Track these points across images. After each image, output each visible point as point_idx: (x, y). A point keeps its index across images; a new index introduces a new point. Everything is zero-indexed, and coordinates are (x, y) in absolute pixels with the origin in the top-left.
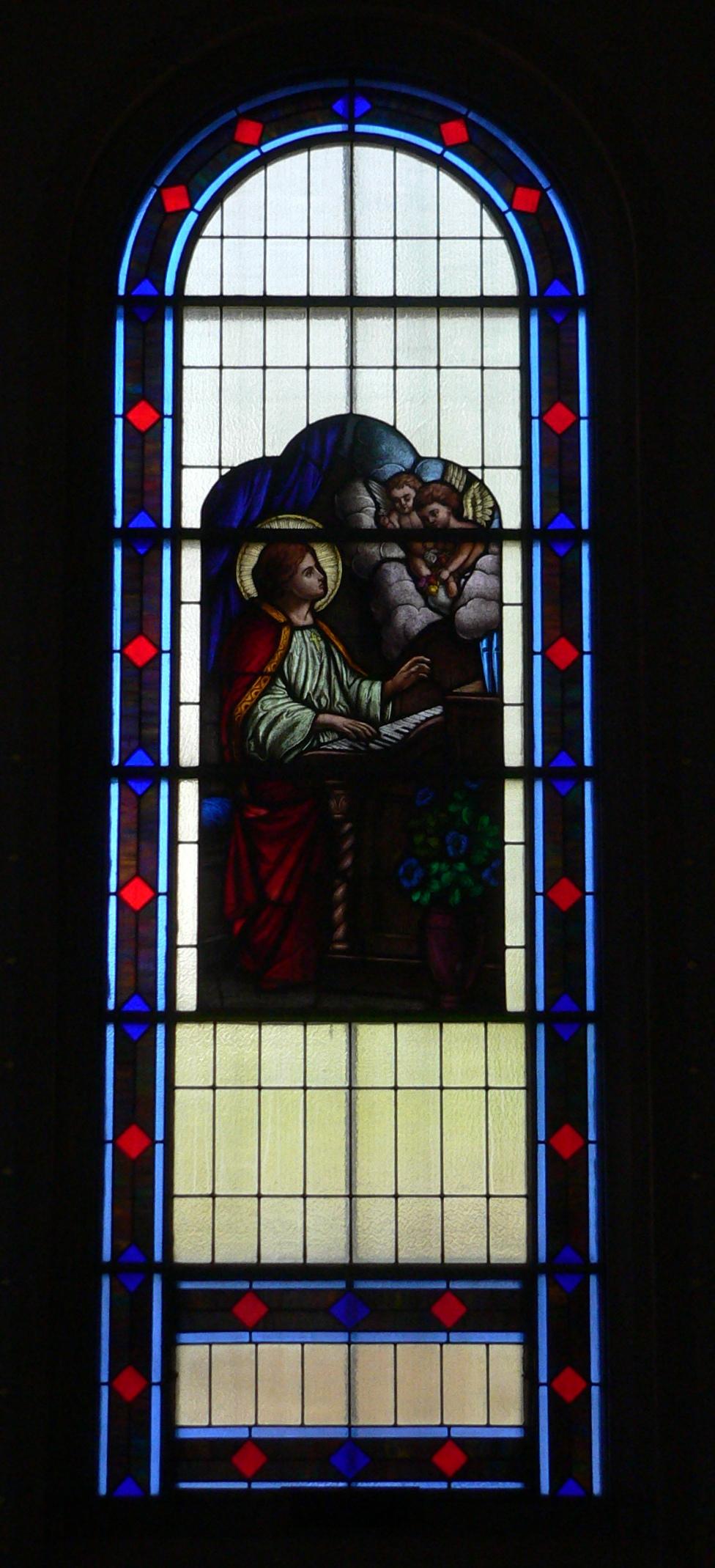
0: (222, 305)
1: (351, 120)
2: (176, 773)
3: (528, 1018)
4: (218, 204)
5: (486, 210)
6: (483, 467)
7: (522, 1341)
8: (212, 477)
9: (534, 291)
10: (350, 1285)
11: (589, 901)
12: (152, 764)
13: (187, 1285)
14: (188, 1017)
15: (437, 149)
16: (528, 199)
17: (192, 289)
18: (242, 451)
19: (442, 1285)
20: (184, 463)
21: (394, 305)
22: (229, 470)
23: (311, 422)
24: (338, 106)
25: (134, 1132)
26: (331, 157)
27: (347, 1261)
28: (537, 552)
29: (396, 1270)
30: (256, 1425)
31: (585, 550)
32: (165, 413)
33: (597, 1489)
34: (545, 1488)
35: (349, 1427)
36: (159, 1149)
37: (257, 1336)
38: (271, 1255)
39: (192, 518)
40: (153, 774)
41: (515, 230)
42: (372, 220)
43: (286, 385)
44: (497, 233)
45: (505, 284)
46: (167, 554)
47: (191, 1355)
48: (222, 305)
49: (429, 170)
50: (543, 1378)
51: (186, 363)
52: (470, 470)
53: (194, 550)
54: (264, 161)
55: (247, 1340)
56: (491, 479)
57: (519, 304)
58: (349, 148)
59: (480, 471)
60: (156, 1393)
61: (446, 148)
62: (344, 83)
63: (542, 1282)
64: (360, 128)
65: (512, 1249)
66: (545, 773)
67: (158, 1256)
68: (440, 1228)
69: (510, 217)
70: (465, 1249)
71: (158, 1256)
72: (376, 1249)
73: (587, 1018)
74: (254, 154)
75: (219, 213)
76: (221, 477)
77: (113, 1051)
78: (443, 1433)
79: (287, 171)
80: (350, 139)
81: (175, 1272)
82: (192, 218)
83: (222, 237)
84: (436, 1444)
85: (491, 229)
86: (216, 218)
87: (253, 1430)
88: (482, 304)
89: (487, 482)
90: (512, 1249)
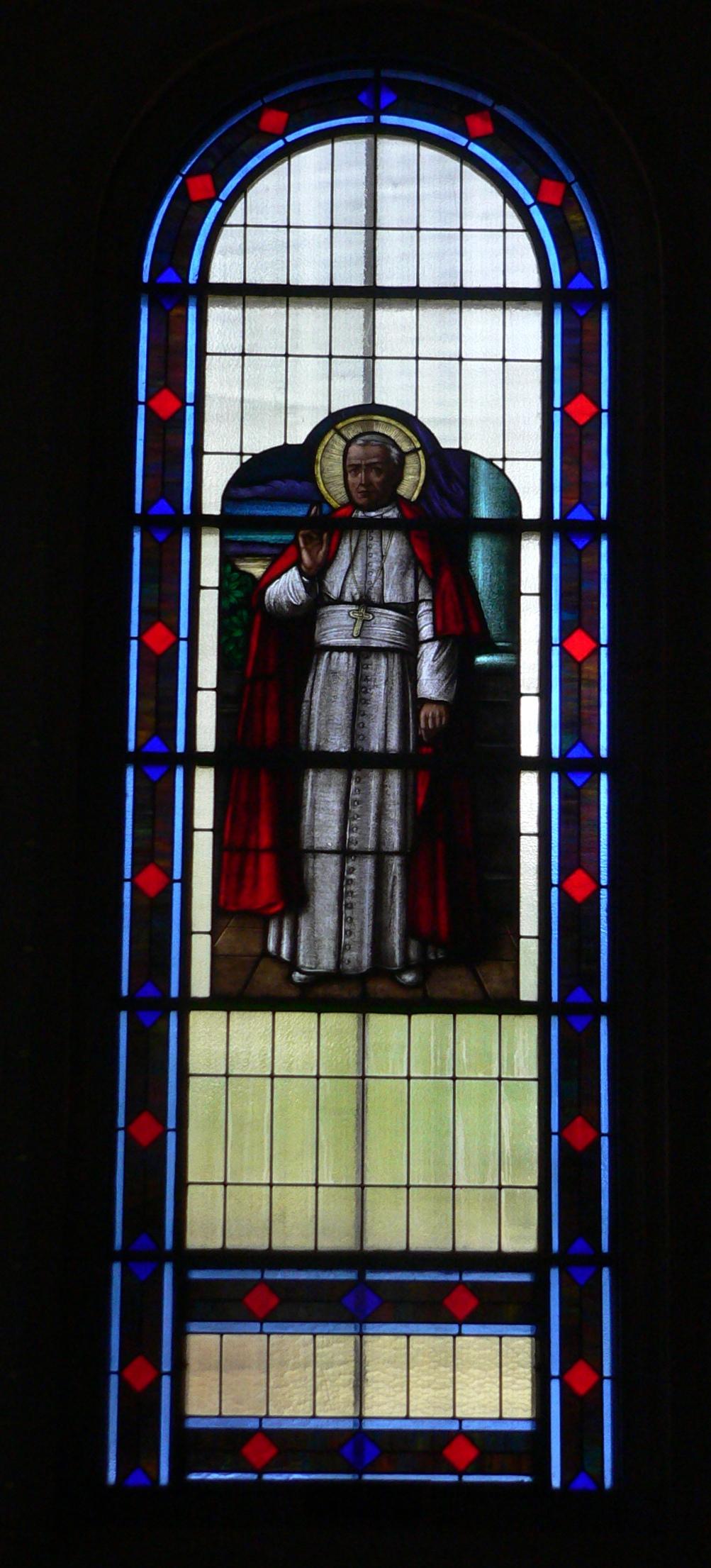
0: (245, 293)
1: (377, 112)
2: (193, 759)
3: (541, 1009)
5: (509, 205)
6: (504, 459)
8: (233, 465)
10: (361, 1276)
11: (605, 1142)
12: (173, 513)
13: (196, 1275)
14: (202, 1005)
16: (553, 192)
17: (216, 276)
18: (263, 439)
21: (415, 296)
23: (333, 411)
24: (363, 97)
25: (145, 1119)
26: (351, 151)
30: (267, 1416)
33: (608, 1482)
34: (556, 1482)
35: (361, 1334)
36: (190, 411)
37: (267, 1327)
38: (282, 1242)
39: (212, 504)
40: (170, 760)
43: (308, 376)
44: (519, 226)
45: (527, 277)
46: (186, 541)
47: (201, 1344)
48: (245, 293)
49: (452, 164)
50: (555, 1370)
51: (192, 1070)
54: (288, 152)
55: (258, 1330)
56: (511, 470)
57: (542, 296)
58: (372, 139)
60: (166, 1382)
62: (369, 73)
63: (554, 1275)
64: (387, 119)
66: (562, 1010)
67: (169, 1243)
71: (169, 1243)
76: (242, 464)
77: (128, 943)
78: (454, 1426)
79: (310, 163)
80: (375, 131)
81: (188, 1259)
82: (217, 206)
83: (243, 354)
84: (448, 1436)
85: (514, 221)
86: (240, 206)
87: (264, 1420)
89: (507, 472)
90: (522, 1239)
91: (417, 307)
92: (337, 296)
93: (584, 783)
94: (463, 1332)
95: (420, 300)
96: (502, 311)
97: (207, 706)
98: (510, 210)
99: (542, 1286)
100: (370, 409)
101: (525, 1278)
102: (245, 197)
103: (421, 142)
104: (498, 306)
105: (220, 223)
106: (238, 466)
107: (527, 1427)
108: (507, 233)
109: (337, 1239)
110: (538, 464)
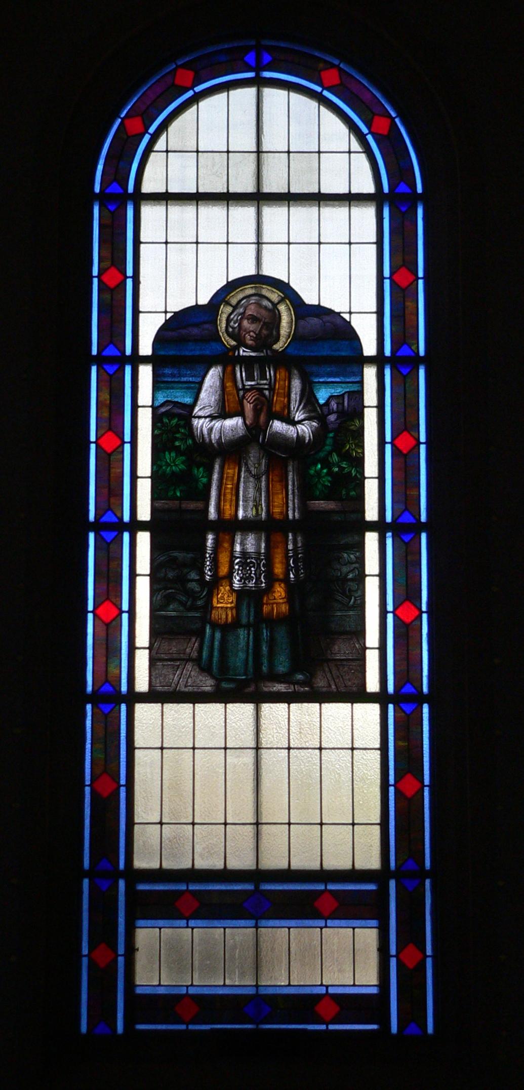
0: (166, 198)
1: (258, 69)
2: (135, 526)
3: (381, 698)
4: (164, 128)
5: (353, 135)
6: (350, 313)
7: (377, 925)
8: (160, 320)
9: (386, 189)
10: (257, 887)
13: (141, 887)
15: (318, 89)
16: (382, 126)
17: (147, 188)
18: (178, 304)
19: (321, 887)
20: (141, 309)
21: (288, 198)
22: (173, 314)
23: (229, 280)
24: (250, 58)
26: (247, 94)
27: (254, 867)
28: (388, 372)
29: (288, 875)
30: (192, 985)
31: (422, 373)
32: (128, 275)
33: (430, 1029)
34: (394, 1029)
35: (257, 927)
36: (123, 790)
39: (146, 349)
40: (121, 360)
41: (388, 678)
42: (274, 140)
48: (166, 198)
49: (314, 104)
50: (393, 951)
52: (342, 315)
53: (149, 367)
57: (377, 199)
59: (348, 315)
61: (324, 88)
62: (253, 43)
63: (392, 884)
64: (267, 74)
65: (370, 860)
67: (122, 866)
68: (320, 852)
69: (370, 138)
70: (337, 861)
72: (274, 861)
73: (425, 874)
74: (190, 94)
75: (165, 135)
76: (166, 320)
78: (323, 991)
80: (259, 83)
82: (147, 138)
84: (319, 997)
85: (356, 146)
86: (163, 138)
87: (189, 988)
88: (350, 199)
89: (353, 324)
90: (370, 860)
91: (319, 207)
92: (171, 199)
93: (411, 540)
94: (328, 925)
95: (169, 202)
96: (317, 208)
97: (145, 488)
98: (353, 139)
99: (383, 892)
100: (258, 279)
101: (372, 887)
102: (167, 131)
103: (290, 89)
104: (345, 206)
105: (149, 149)
106: (163, 321)
107: (375, 991)
108: (352, 154)
109: (241, 861)
110: (374, 316)
